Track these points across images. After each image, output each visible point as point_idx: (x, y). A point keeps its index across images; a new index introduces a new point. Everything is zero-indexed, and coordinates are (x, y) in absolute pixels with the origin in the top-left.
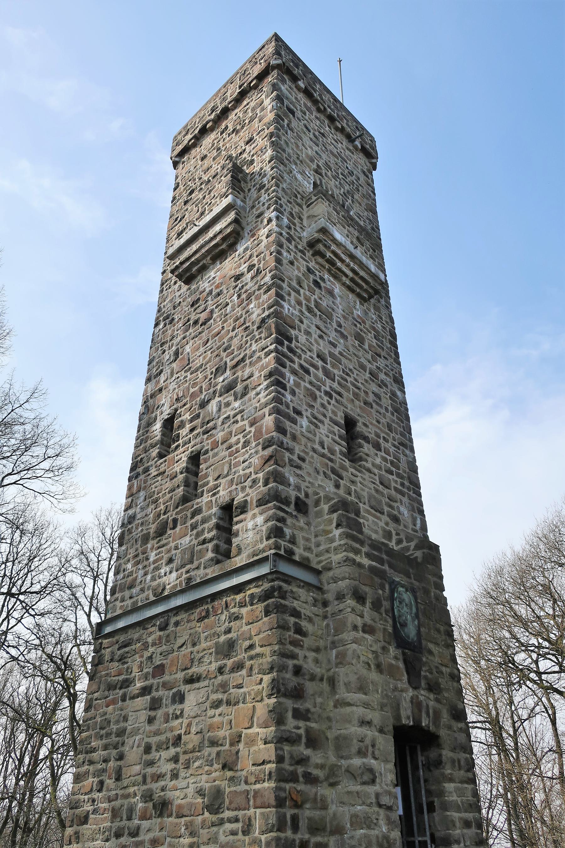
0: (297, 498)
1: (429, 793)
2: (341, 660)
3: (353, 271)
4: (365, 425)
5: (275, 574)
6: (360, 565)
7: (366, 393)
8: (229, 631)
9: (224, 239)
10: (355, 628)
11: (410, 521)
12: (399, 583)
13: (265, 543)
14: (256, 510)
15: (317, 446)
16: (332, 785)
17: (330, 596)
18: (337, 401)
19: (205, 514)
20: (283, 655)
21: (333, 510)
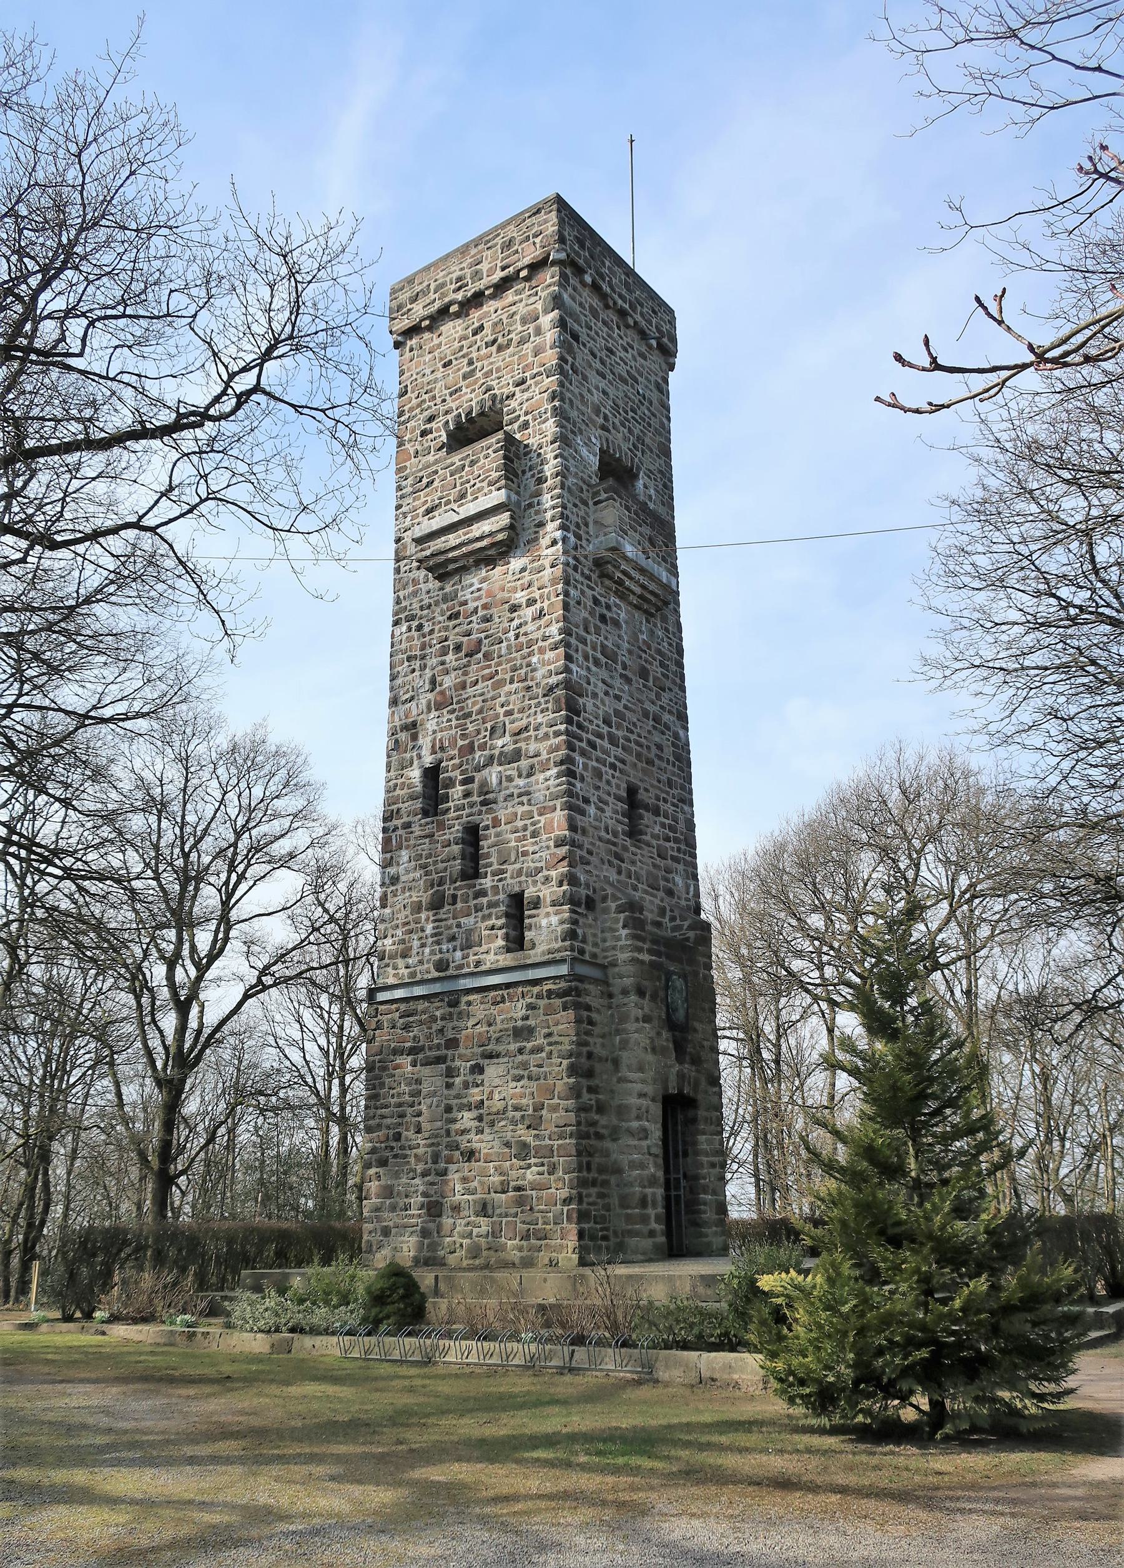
0: (587, 896)
1: (685, 1143)
2: (624, 1045)
3: (643, 587)
4: (646, 790)
5: (573, 977)
6: (642, 962)
7: (648, 748)
9: (493, 545)
10: (637, 1020)
11: (683, 890)
12: (674, 973)
13: (560, 944)
14: (550, 909)
15: (603, 834)
16: (615, 1140)
17: (615, 990)
18: (621, 771)
19: (491, 898)
20: (580, 1044)
21: (620, 909)
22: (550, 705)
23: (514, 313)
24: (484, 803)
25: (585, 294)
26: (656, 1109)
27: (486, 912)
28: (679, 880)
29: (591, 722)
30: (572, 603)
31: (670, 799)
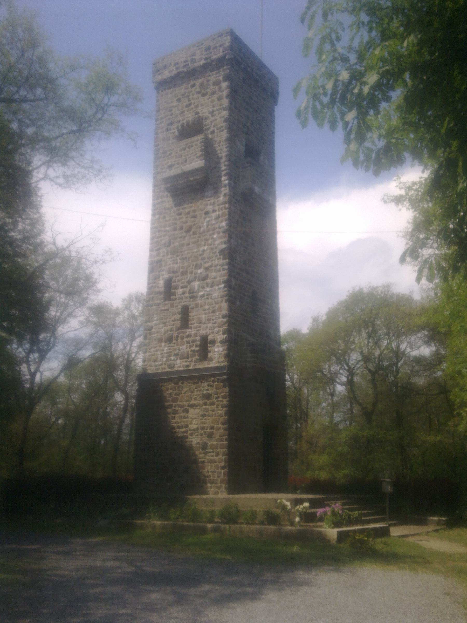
8: (208, 390)
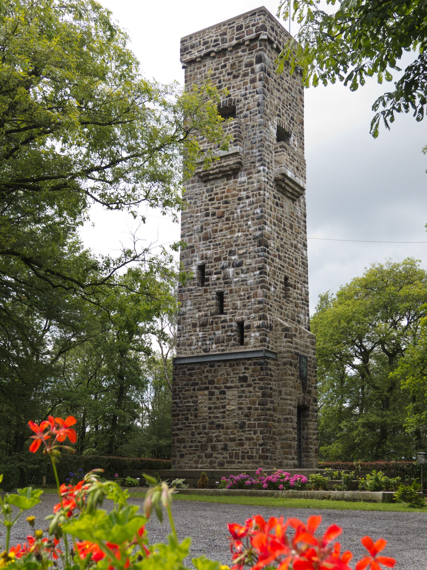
3: (293, 189)
4: (291, 278)
11: (304, 321)
22: (256, 243)
23: (242, 61)
24: (225, 283)
25: (273, 53)
26: (295, 411)
27: (227, 329)
28: (302, 316)
29: (272, 250)
30: (266, 198)
31: (300, 282)
